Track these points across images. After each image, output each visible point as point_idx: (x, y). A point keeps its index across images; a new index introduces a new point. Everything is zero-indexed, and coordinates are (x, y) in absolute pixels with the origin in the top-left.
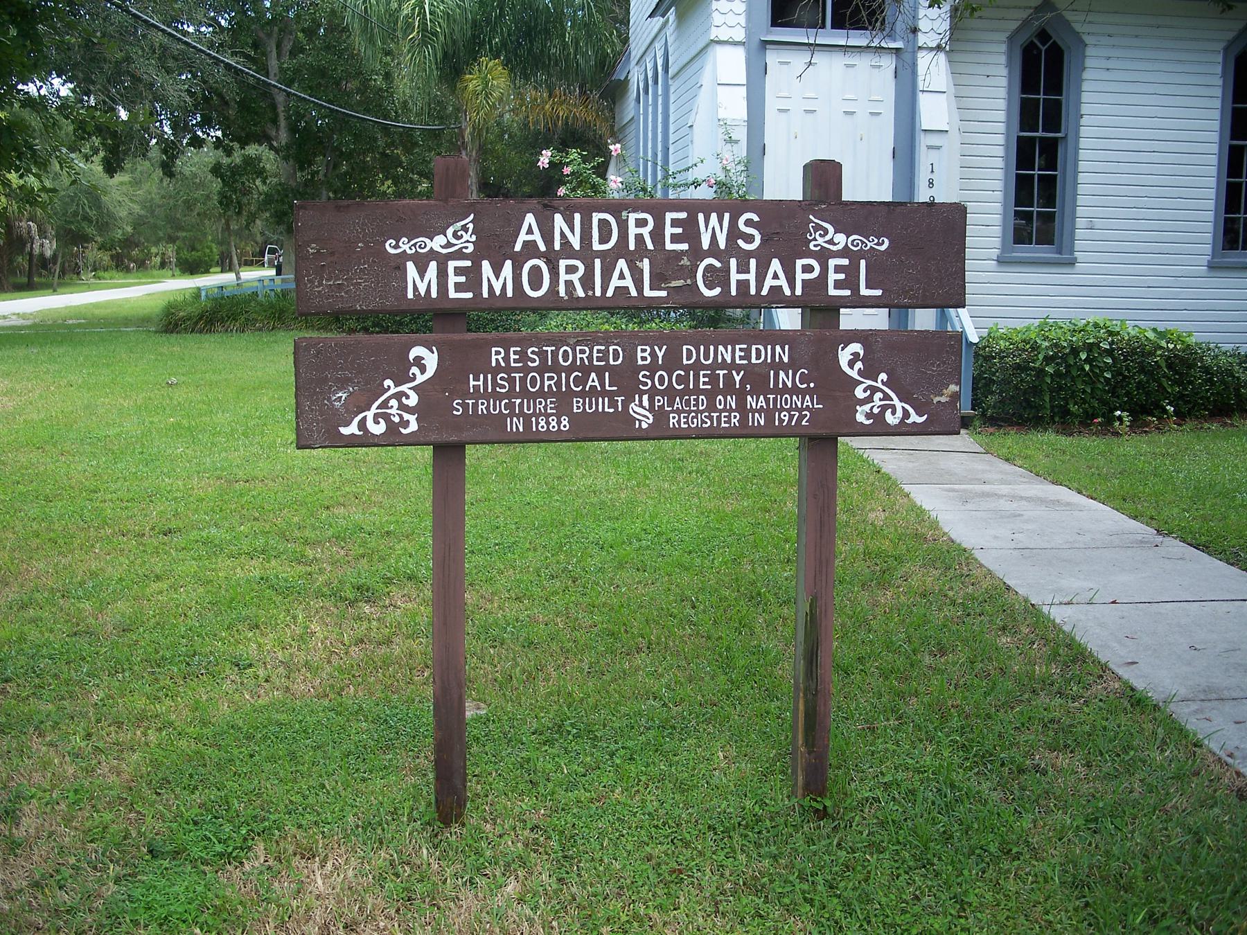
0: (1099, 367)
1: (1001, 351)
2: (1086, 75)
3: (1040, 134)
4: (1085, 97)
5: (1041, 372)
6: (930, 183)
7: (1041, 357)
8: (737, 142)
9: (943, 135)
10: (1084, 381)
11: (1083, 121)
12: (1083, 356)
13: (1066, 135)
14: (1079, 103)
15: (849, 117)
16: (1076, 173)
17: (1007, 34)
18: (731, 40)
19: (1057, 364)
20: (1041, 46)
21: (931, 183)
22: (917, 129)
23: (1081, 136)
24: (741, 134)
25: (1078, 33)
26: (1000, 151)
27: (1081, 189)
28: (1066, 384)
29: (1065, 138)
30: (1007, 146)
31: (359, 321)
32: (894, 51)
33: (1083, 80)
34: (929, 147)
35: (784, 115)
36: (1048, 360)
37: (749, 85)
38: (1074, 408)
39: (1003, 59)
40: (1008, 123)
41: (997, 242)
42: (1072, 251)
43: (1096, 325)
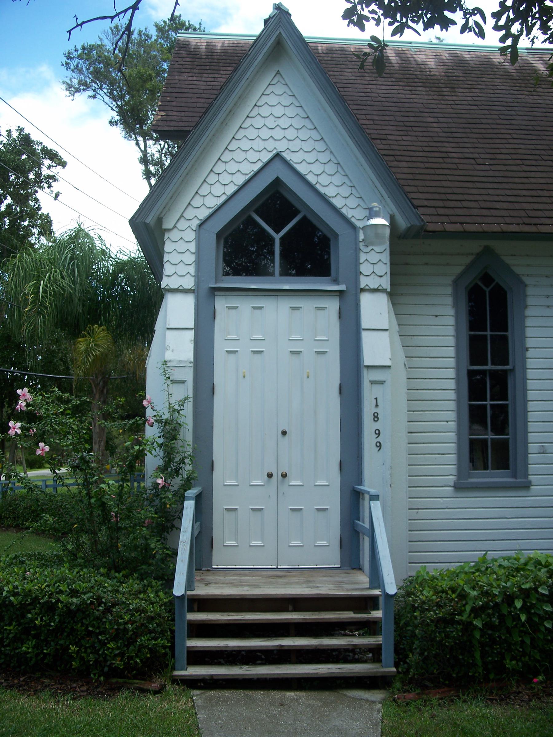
0: (539, 615)
1: (424, 602)
2: (528, 312)
3: (489, 367)
4: (529, 332)
5: (468, 627)
6: (375, 417)
7: (468, 608)
8: (183, 382)
9: (387, 371)
10: (521, 631)
11: (529, 354)
12: (518, 604)
13: (514, 367)
14: (523, 337)
15: (294, 357)
16: (525, 401)
17: (453, 278)
18: (180, 288)
19: (489, 615)
20: (484, 288)
21: (376, 417)
22: (362, 366)
23: (528, 367)
24: (188, 375)
25: (518, 275)
26: (452, 384)
27: (531, 416)
28: (500, 637)
29: (513, 370)
30: (458, 380)
31: (15, 519)
32: (338, 294)
33: (526, 317)
34: (373, 382)
35: (232, 356)
36: (476, 612)
37: (197, 328)
38: (510, 664)
39: (449, 300)
40: (458, 357)
41: (453, 469)
42: (526, 474)
43: (538, 563)
